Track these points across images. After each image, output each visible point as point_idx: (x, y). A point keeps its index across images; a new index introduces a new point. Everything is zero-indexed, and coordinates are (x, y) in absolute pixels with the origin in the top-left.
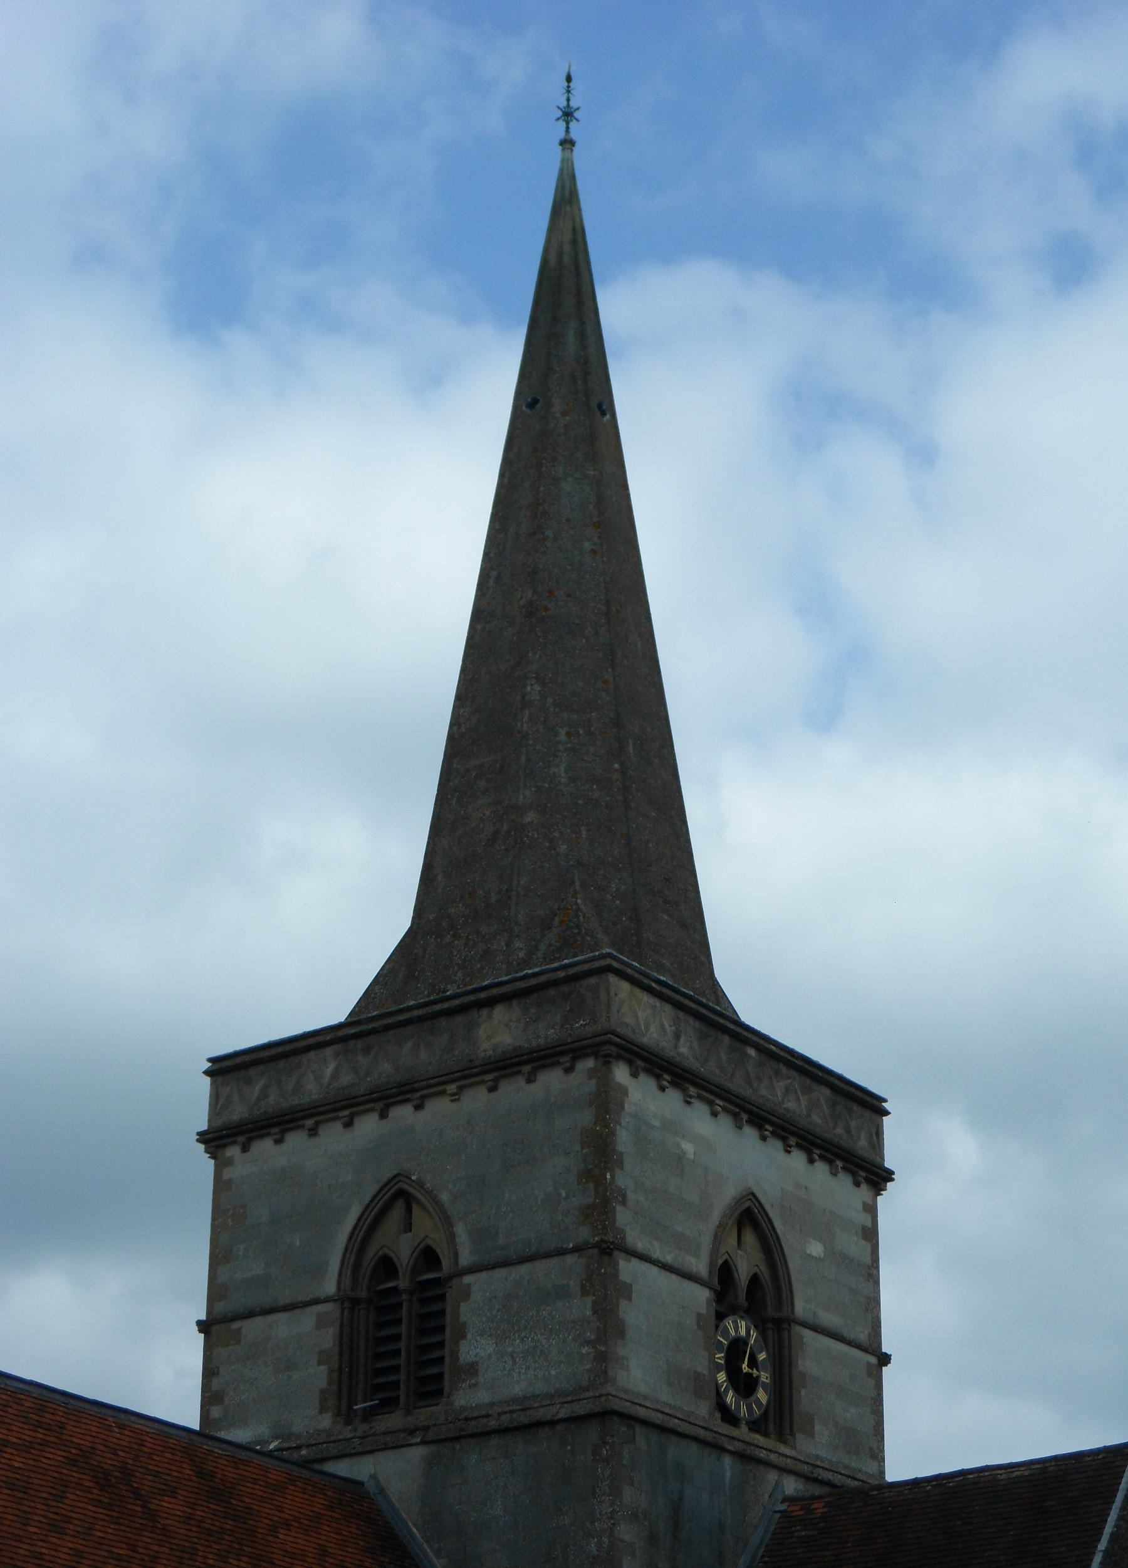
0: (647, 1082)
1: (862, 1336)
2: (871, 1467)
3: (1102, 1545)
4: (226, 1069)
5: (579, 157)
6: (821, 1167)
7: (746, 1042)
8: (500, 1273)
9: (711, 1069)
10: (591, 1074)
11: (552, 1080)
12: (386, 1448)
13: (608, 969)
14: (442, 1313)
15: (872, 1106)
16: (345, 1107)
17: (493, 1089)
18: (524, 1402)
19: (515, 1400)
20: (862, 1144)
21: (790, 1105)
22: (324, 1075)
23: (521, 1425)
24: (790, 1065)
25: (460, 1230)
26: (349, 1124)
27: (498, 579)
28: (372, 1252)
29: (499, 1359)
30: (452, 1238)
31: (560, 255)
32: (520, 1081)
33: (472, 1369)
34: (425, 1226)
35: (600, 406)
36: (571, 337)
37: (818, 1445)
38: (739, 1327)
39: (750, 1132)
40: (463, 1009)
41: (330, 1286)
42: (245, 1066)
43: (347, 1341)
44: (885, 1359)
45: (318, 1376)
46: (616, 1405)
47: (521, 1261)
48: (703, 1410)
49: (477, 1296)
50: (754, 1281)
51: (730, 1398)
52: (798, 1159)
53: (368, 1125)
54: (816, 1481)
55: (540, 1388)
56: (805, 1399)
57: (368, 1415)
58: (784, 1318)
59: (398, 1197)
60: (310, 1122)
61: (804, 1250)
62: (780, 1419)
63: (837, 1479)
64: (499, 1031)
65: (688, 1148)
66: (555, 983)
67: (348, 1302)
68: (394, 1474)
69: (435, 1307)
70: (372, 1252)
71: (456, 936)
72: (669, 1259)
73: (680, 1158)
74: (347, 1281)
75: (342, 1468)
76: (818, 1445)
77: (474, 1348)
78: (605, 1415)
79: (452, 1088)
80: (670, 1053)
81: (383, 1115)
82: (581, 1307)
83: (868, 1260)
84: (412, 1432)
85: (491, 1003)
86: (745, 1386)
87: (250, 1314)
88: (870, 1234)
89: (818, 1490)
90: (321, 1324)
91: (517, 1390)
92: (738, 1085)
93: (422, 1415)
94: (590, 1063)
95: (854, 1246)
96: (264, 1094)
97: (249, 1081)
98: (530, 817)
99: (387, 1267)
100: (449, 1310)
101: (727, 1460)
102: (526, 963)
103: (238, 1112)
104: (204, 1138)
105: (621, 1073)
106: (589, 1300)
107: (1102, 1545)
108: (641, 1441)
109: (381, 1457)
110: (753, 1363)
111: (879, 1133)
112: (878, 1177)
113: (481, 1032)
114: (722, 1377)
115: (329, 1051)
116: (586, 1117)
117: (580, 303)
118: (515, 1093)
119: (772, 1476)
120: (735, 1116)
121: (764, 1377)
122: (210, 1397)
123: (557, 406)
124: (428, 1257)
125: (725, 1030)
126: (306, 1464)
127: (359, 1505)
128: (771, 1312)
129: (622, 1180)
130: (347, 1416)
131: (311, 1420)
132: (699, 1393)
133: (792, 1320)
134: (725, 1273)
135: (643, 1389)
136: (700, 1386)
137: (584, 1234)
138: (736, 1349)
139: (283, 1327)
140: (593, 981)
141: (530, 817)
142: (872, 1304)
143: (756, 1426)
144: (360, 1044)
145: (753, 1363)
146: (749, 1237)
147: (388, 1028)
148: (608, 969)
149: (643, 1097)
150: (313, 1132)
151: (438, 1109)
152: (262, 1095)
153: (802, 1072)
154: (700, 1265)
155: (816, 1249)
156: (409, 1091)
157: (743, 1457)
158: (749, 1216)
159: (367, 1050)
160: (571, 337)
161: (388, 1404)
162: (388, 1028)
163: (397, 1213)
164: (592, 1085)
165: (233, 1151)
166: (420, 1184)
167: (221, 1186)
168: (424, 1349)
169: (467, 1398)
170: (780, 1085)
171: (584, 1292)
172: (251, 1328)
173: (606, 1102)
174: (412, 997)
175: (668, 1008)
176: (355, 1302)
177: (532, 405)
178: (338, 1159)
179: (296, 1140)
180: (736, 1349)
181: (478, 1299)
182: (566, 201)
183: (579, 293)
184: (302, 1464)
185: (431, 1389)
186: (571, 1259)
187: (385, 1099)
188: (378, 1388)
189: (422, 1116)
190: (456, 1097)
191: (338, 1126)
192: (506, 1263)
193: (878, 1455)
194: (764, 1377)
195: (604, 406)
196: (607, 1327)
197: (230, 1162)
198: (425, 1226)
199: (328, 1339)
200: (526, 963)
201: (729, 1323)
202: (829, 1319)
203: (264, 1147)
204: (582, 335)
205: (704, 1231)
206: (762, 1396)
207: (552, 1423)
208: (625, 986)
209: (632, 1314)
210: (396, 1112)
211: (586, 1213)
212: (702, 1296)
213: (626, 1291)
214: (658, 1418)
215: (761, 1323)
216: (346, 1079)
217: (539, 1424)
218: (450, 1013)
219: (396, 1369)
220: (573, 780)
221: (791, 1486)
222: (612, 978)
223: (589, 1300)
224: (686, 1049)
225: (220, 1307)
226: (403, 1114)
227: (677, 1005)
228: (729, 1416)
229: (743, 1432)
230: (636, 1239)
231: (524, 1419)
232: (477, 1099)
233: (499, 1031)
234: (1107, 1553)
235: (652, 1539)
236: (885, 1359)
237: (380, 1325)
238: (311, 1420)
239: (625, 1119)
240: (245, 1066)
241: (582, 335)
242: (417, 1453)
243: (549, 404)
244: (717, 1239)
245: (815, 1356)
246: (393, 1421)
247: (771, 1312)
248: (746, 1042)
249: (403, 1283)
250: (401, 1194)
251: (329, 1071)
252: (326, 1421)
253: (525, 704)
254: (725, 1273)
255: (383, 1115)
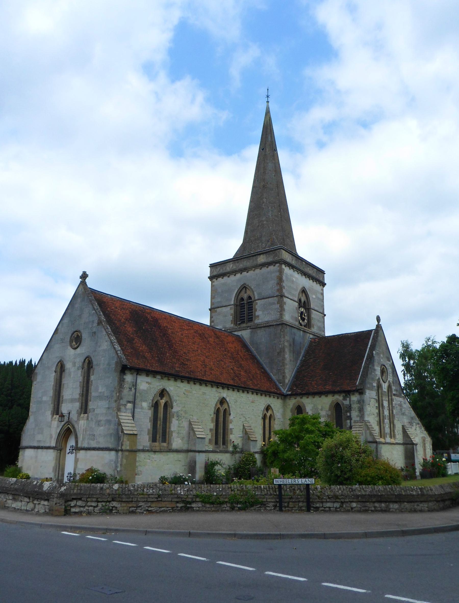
0: (287, 268)
1: (321, 311)
2: (323, 333)
3: (369, 346)
4: (212, 266)
5: (270, 104)
6: (315, 283)
7: (303, 261)
8: (263, 300)
9: (297, 266)
10: (278, 266)
11: (271, 268)
12: (244, 330)
13: (281, 248)
14: (252, 307)
15: (322, 272)
16: (234, 272)
17: (261, 269)
18: (268, 322)
19: (266, 321)
20: (321, 279)
21: (310, 272)
22: (230, 267)
23: (267, 326)
24: (310, 265)
25: (255, 293)
26: (235, 275)
27: (258, 181)
28: (240, 297)
29: (262, 315)
30: (254, 294)
31: (267, 122)
32: (266, 268)
33: (258, 316)
34: (249, 293)
35: (274, 150)
36: (269, 137)
37: (314, 330)
38: (302, 310)
39: (304, 277)
40: (255, 255)
41: (232, 303)
42: (216, 265)
43: (236, 312)
44: (325, 315)
45: (231, 318)
46: (284, 322)
47: (268, 298)
48: (297, 323)
49: (259, 304)
50: (304, 302)
51: (301, 321)
52: (311, 281)
53: (238, 275)
54: (315, 335)
55: (270, 319)
56: (313, 322)
57: (240, 324)
58: (308, 307)
59: (244, 287)
60: (228, 275)
61: (312, 297)
62: (309, 325)
63: (318, 335)
64: (262, 259)
65: (294, 279)
66: (272, 251)
67: (236, 305)
68: (245, 334)
69: (251, 306)
70: (240, 297)
71: (252, 243)
72: (291, 298)
73: (293, 281)
74: (235, 301)
75: (236, 333)
76: (314, 330)
77: (258, 313)
78: (283, 324)
79: (253, 269)
80: (291, 263)
81: (241, 274)
82: (278, 306)
83: (322, 298)
84: (248, 327)
85: (260, 254)
86: (303, 319)
87: (218, 307)
88: (322, 294)
89: (315, 337)
90: (231, 309)
91: (266, 320)
92: (302, 268)
93: (249, 324)
94: (278, 265)
95: (320, 296)
96: (220, 270)
97: (217, 268)
98: (265, 222)
99: (242, 299)
100: (254, 307)
101: (301, 332)
102: (265, 248)
103: (215, 273)
104: (209, 278)
105: (283, 266)
106: (279, 305)
107: (369, 346)
108: (288, 328)
109: (243, 331)
110: (304, 316)
111: (324, 277)
112: (324, 284)
113: (259, 259)
114: (300, 318)
115: (231, 263)
116: (278, 274)
117: (271, 131)
118: (265, 270)
119: (308, 335)
120: (301, 274)
121: (306, 318)
122: (211, 321)
123: (267, 150)
124: (250, 298)
125: (300, 259)
126: (231, 332)
127: (240, 339)
128: (307, 307)
129: (284, 285)
130: (236, 324)
131: (229, 325)
132: (296, 321)
133: (310, 308)
134: (300, 300)
135: (288, 320)
136: (296, 319)
137: (278, 294)
138: (302, 313)
139: (224, 309)
140: (278, 250)
141: (265, 222)
142: (323, 306)
143: (305, 326)
144: (237, 261)
145: (304, 316)
146: (304, 294)
147: (242, 259)
148: (281, 248)
149: (287, 271)
150: (229, 277)
151: (251, 272)
152: (219, 271)
153: (312, 266)
154: (296, 299)
155: (314, 297)
156: (246, 269)
157: (304, 331)
158: (304, 291)
159: (238, 263)
160: (269, 137)
161: (243, 322)
162: (242, 259)
163: (244, 290)
164: (279, 268)
165: (214, 280)
166: (248, 285)
167: (212, 286)
168: (249, 313)
169: (257, 321)
170: (308, 269)
171: (278, 303)
172: (218, 310)
173: (281, 271)
174: (237, 259)
175: (291, 255)
176: (237, 305)
177: (263, 150)
178: (234, 282)
179: (226, 278)
180: (302, 313)
181: (259, 305)
182: (268, 113)
183: (271, 130)
184: (230, 332)
185: (250, 320)
186: (275, 298)
187: (241, 271)
188: (241, 320)
189: (248, 274)
190: (254, 270)
191: (233, 275)
192: (264, 299)
193: (324, 331)
194: (306, 318)
195: (275, 150)
196: (282, 309)
197: (214, 282)
198: (249, 293)
199: (232, 312)
200: (265, 248)
201: (300, 309)
202: (316, 308)
203: (220, 279)
204: (271, 137)
205: (297, 293)
206: (306, 321)
207: (273, 325)
208: (284, 251)
209: (286, 307)
210: (243, 273)
211: (278, 290)
212: (296, 304)
213: (285, 303)
214: (291, 325)
215: (305, 309)
216: (234, 267)
217: (271, 326)
218: (253, 256)
219: (244, 316)
220: (272, 216)
221: (311, 336)
222: (282, 250)
223: (279, 305)
224: (294, 262)
225: (213, 306)
226: (245, 273)
227: (292, 255)
228: (301, 325)
229: (303, 327)
230: (286, 294)
231: (268, 325)
232: (258, 271)
233: (262, 259)
234: (370, 348)
235: (290, 345)
236: (325, 315)
237: (241, 309)
238: (229, 325)
239: (284, 274)
240: (216, 265)
241: (271, 137)
242: (249, 331)
243: (266, 150)
244: (299, 295)
245: (314, 315)
246: (244, 325)
247: (307, 307)
248: (303, 261)
249: (245, 302)
250: (245, 287)
251: (231, 266)
252: (232, 325)
253: (263, 203)
254: (300, 300)
255: (241, 274)
